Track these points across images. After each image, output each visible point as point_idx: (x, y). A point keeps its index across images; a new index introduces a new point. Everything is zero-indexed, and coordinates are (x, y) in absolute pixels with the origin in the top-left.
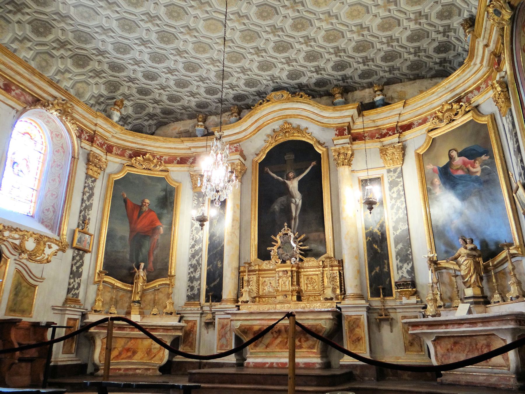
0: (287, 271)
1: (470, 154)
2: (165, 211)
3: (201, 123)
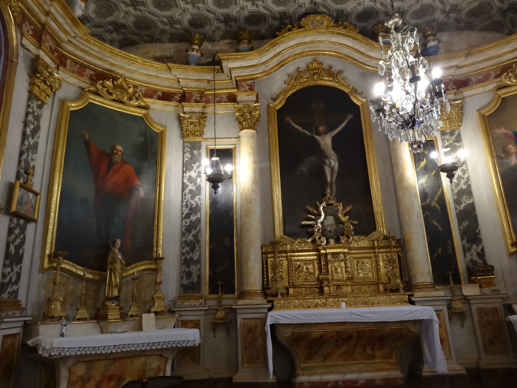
0: (337, 253)
2: (146, 165)
3: (196, 47)
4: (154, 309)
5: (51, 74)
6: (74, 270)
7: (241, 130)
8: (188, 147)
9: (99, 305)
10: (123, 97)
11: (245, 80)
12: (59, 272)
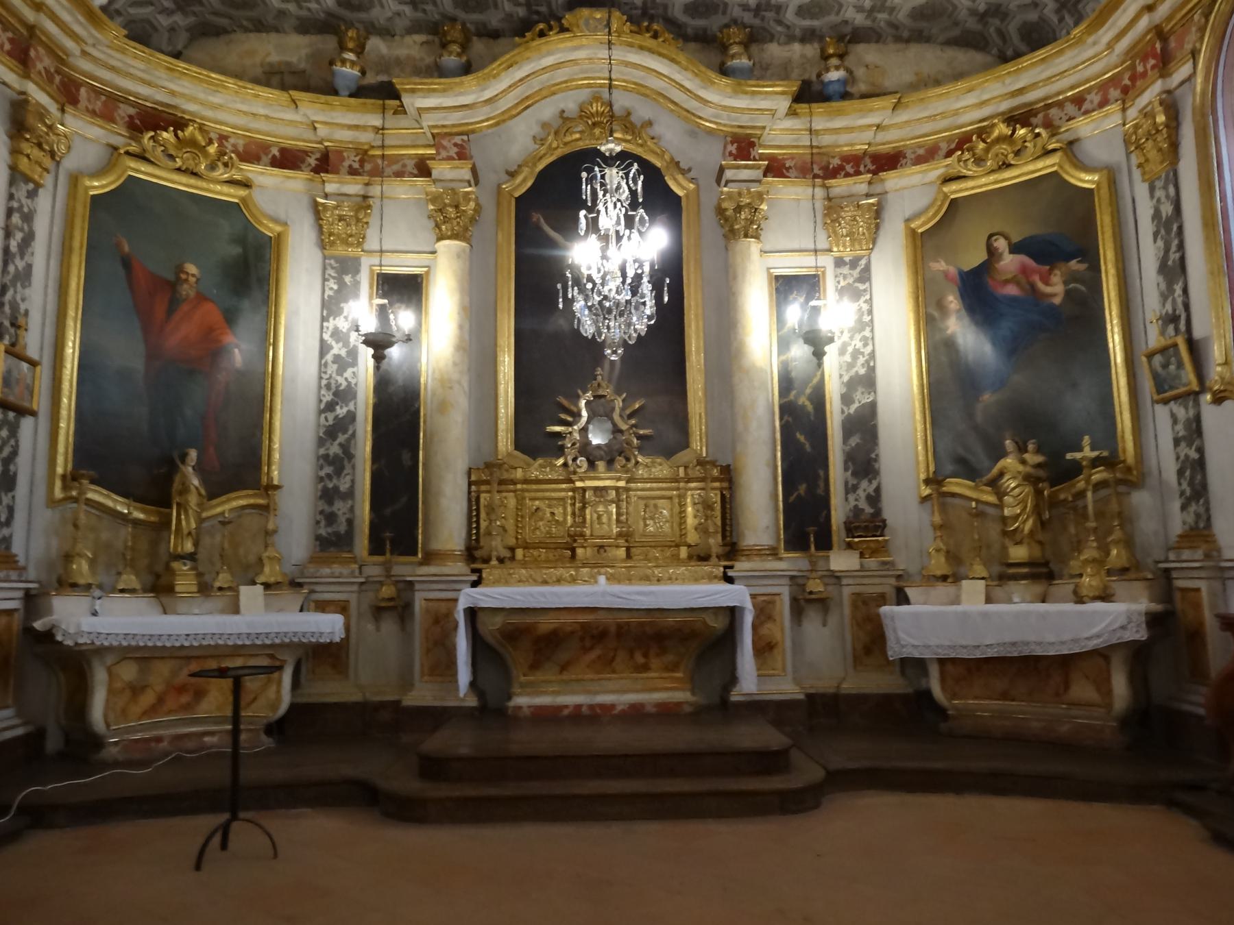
0: (605, 489)
1: (1042, 251)
2: (246, 304)
3: (351, 56)
4: (261, 579)
5: (51, 128)
6: (110, 504)
7: (440, 239)
8: (333, 268)
9: (159, 568)
10: (196, 165)
11: (447, 134)
12: (84, 507)
